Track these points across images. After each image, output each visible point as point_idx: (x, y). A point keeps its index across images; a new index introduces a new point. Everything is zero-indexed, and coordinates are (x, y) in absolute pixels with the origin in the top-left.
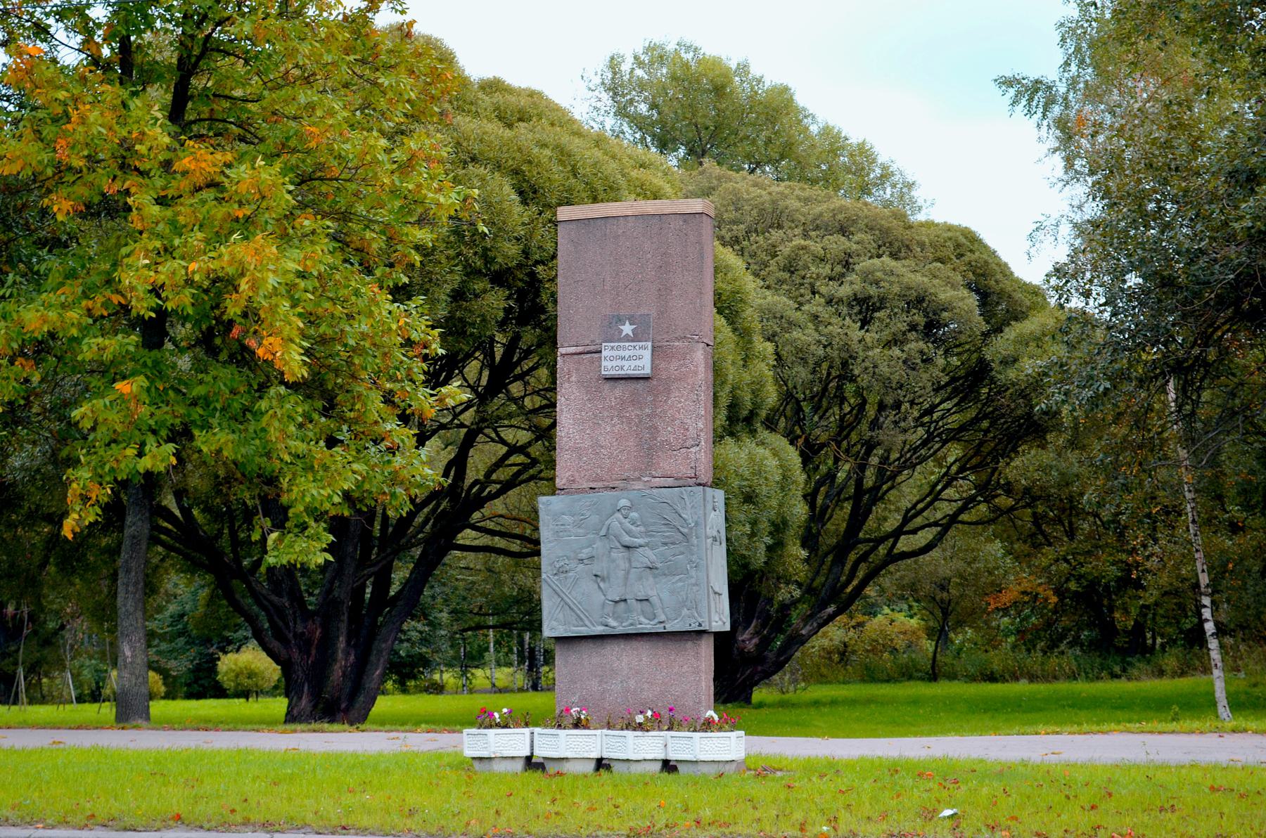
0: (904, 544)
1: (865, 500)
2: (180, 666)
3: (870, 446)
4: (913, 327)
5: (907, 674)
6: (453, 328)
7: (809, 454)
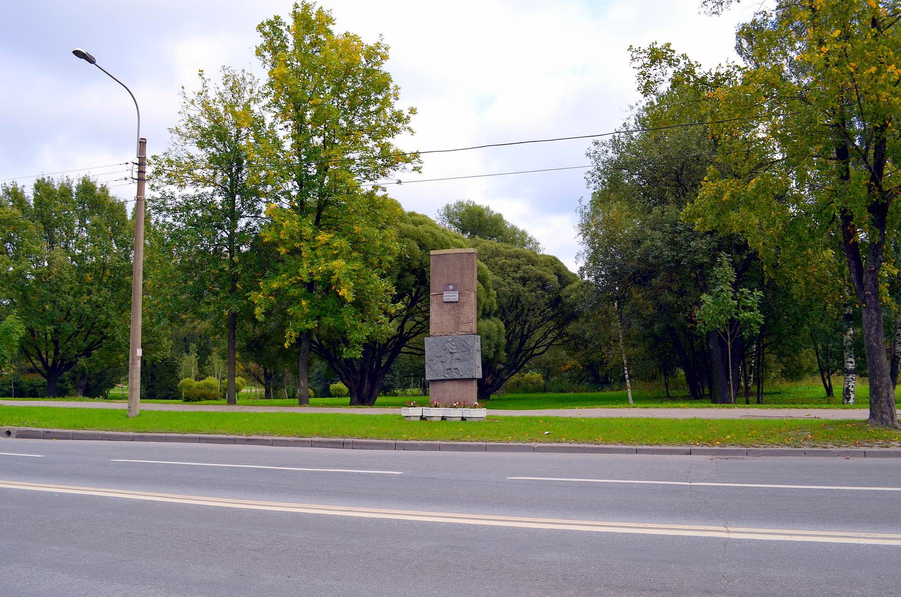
0: (536, 351)
1: (524, 338)
2: (318, 388)
3: (526, 322)
4: (538, 286)
5: (536, 391)
6: (398, 286)
7: (507, 325)
